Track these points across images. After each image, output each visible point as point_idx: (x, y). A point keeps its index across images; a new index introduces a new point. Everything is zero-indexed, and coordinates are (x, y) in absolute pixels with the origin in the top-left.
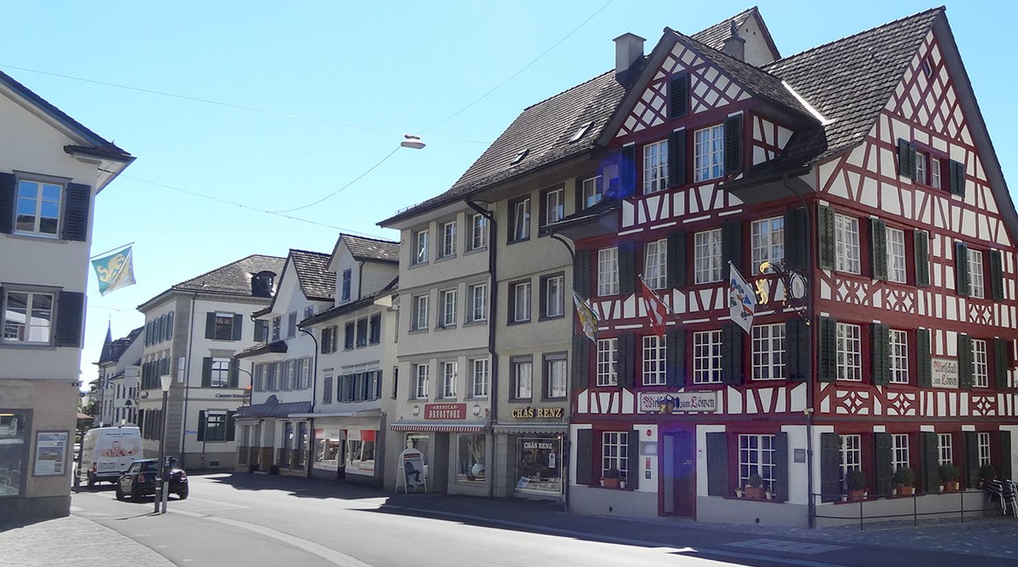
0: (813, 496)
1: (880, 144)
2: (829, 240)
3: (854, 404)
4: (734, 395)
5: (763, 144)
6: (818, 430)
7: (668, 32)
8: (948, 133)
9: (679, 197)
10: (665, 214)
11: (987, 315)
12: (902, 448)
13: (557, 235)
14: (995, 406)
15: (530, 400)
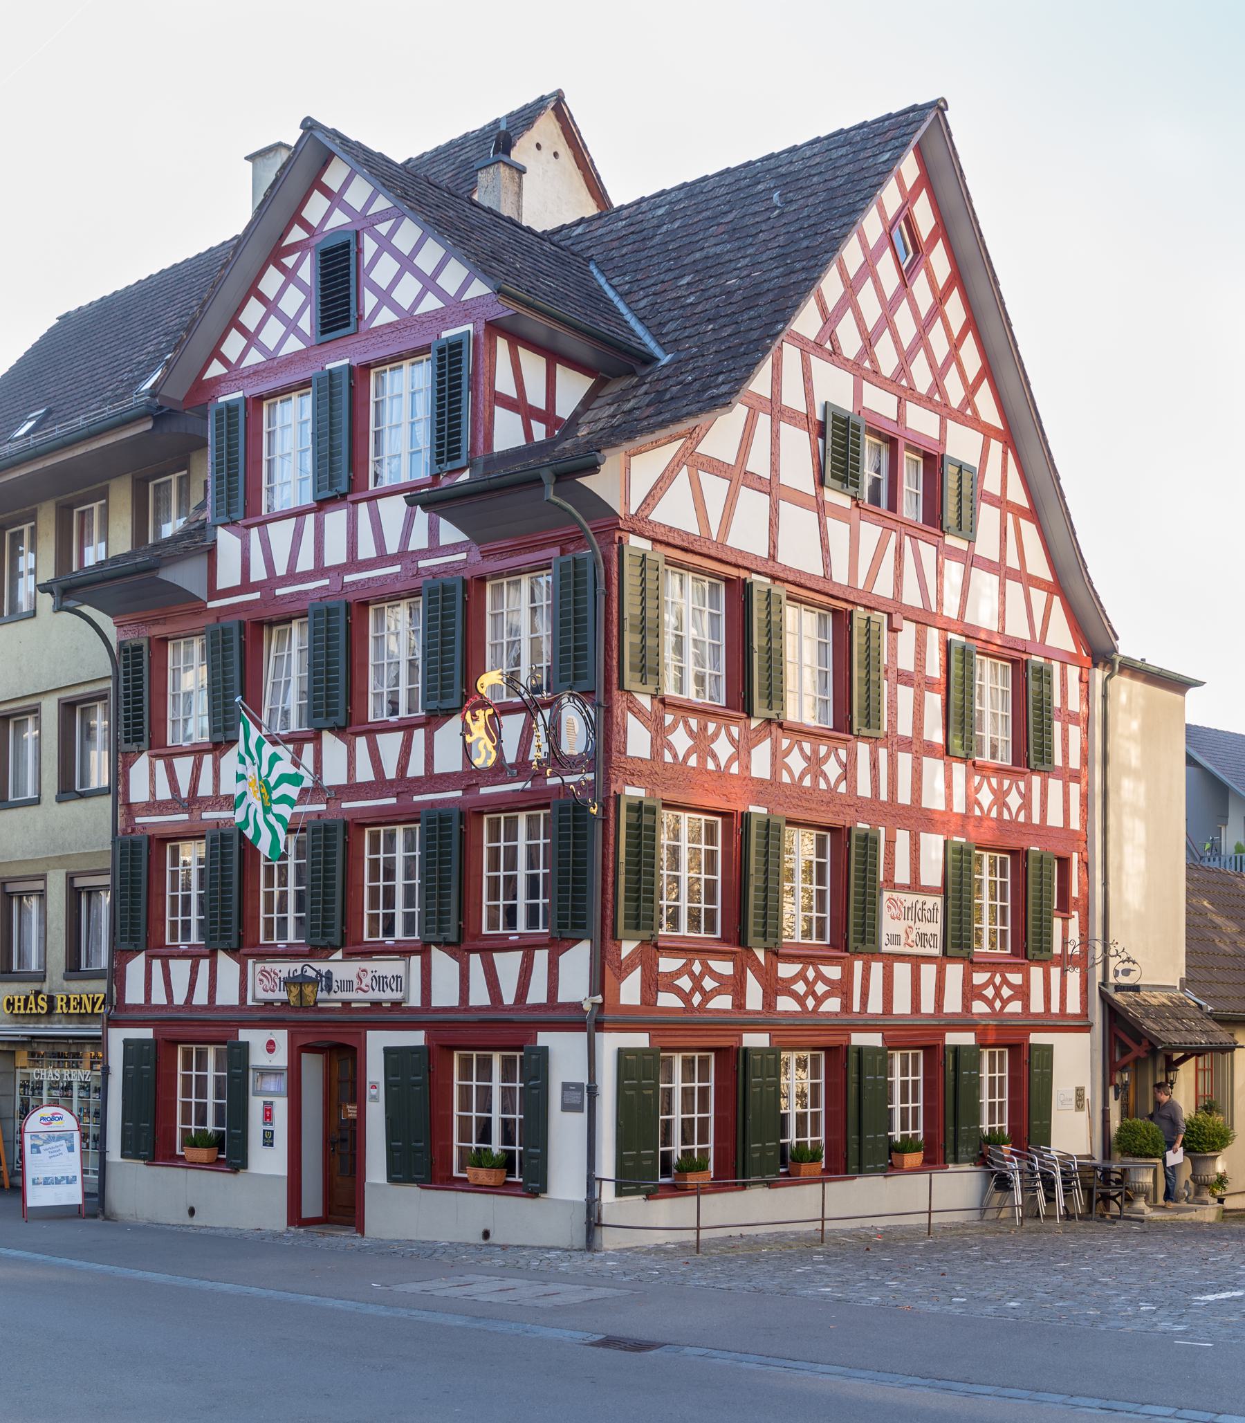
0: (597, 1184)
1: (779, 412)
2: (649, 628)
3: (697, 986)
4: (444, 964)
5: (518, 405)
6: (610, 1043)
7: (310, 128)
8: (944, 395)
9: (336, 520)
10: (306, 562)
11: (1014, 800)
12: (910, 1078)
13: (86, 609)
14: (1023, 993)
15: (41, 977)
